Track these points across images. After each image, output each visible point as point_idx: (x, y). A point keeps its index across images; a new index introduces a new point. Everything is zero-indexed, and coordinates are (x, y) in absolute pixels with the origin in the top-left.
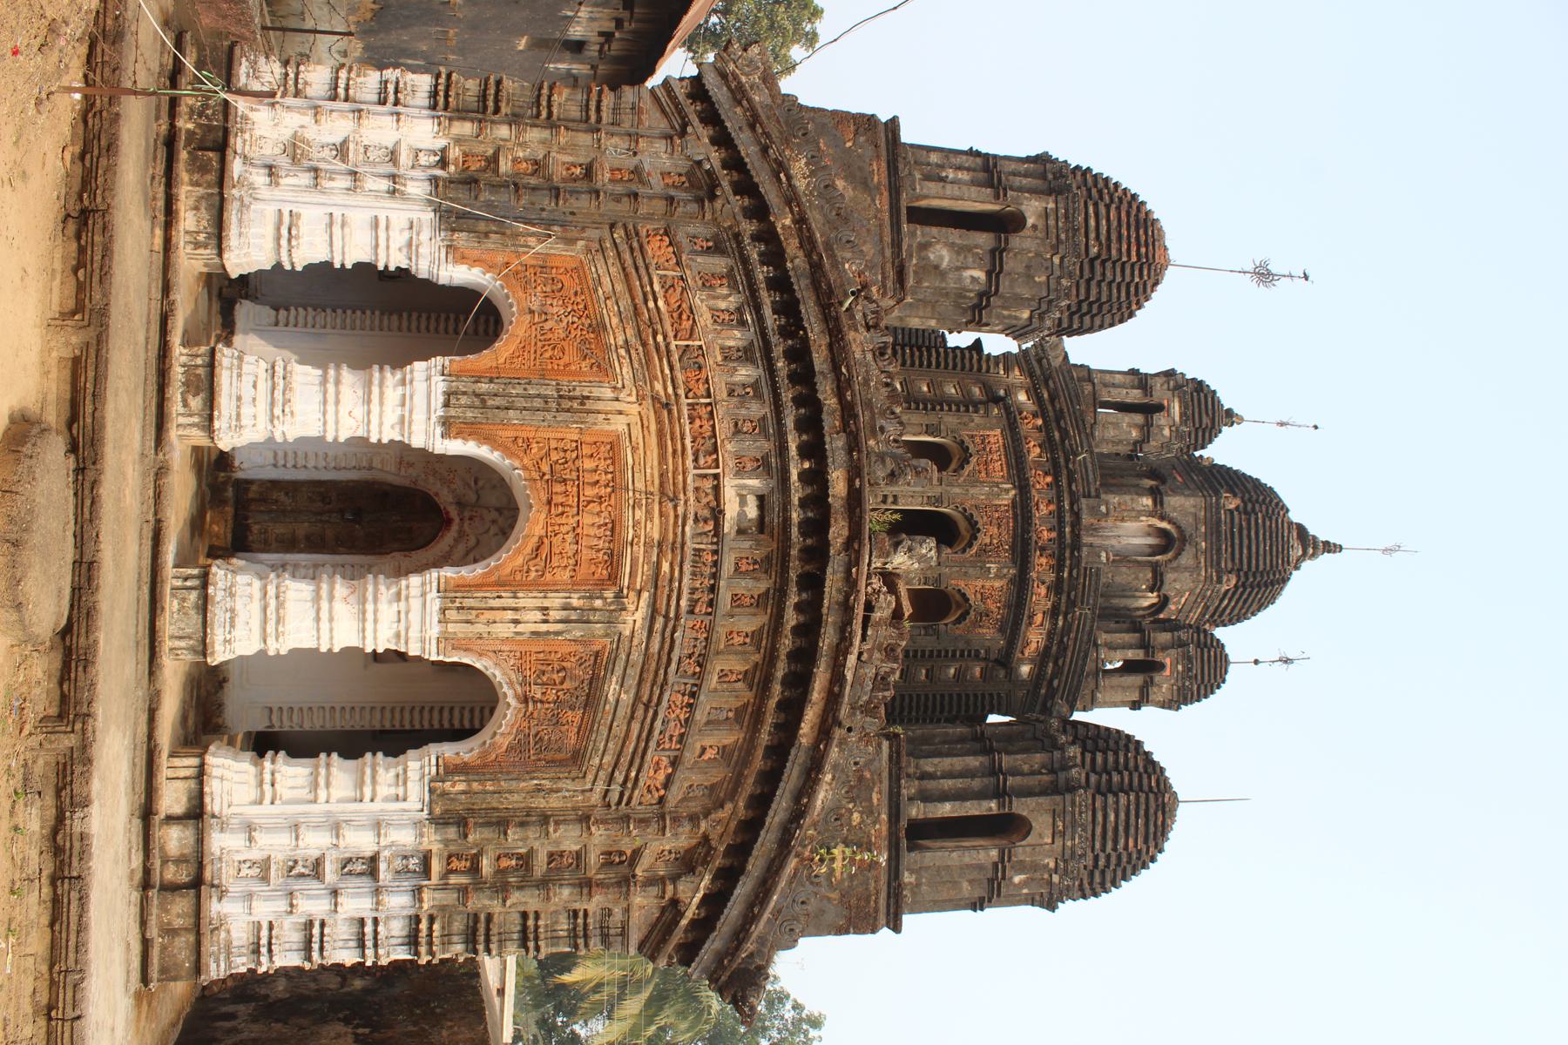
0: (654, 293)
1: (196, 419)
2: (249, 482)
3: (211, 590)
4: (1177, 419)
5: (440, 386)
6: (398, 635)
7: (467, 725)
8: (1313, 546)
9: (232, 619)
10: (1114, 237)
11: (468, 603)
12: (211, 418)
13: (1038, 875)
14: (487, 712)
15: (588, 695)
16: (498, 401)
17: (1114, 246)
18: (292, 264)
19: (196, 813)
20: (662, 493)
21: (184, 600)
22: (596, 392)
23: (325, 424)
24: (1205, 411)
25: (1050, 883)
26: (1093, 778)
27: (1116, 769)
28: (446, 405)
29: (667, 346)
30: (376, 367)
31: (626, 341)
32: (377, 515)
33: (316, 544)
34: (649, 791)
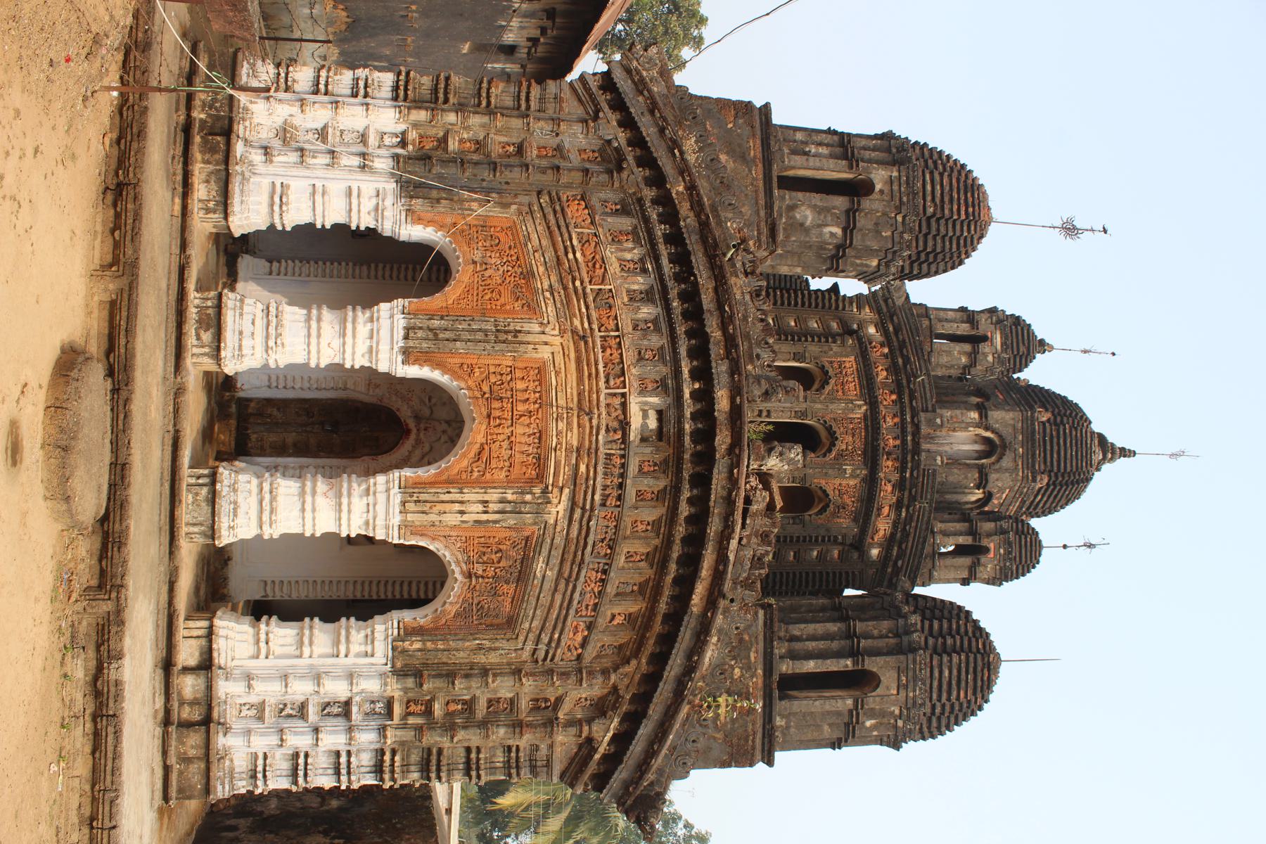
0: (573, 246)
1: (207, 350)
2: (249, 400)
3: (218, 486)
4: (999, 347)
5: (400, 322)
6: (367, 523)
7: (422, 596)
8: (1111, 452)
9: (235, 510)
10: (946, 199)
11: (423, 497)
12: (218, 349)
13: (885, 720)
14: (438, 586)
15: (520, 572)
16: (448, 335)
17: (947, 207)
18: (283, 225)
19: (206, 665)
20: (580, 408)
21: (197, 494)
22: (527, 327)
24: (1022, 341)
25: (896, 727)
26: (931, 641)
27: (950, 634)
28: (406, 337)
29: (584, 289)
30: (350, 307)
31: (551, 286)
32: (350, 426)
33: (301, 450)
34: (569, 650)
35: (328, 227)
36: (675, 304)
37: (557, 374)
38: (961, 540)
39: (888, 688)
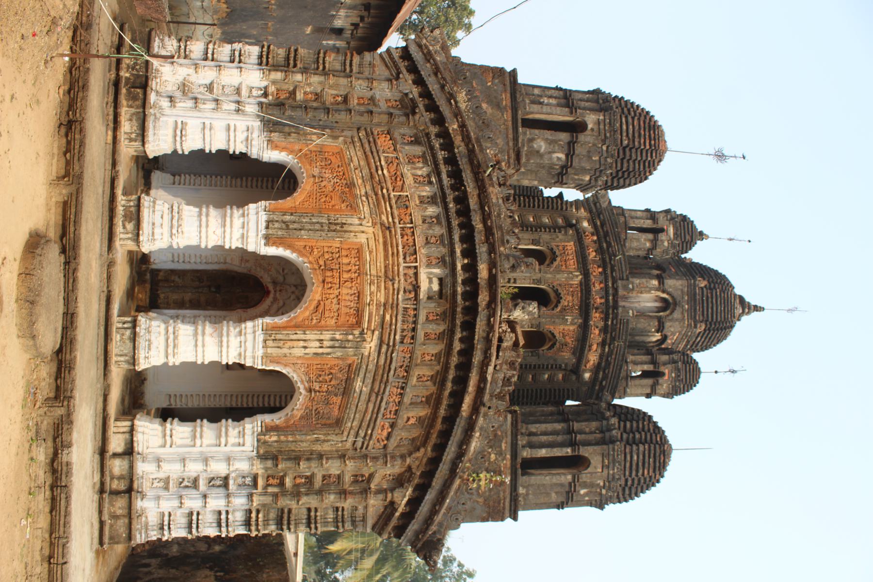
1: (130, 236)
2: (159, 271)
4: (672, 236)
5: (263, 217)
6: (240, 355)
8: (748, 308)
9: (149, 345)
10: (636, 135)
11: (279, 337)
12: (138, 235)
14: (289, 398)
15: (345, 388)
16: (296, 226)
17: (637, 140)
18: (183, 150)
19: (129, 452)
20: (386, 276)
21: (123, 335)
22: (350, 221)
24: (687, 232)
25: (601, 494)
26: (625, 436)
28: (267, 227)
29: (389, 195)
32: (229, 288)
33: (195, 305)
34: (378, 441)
35: (214, 151)
37: (371, 252)
38: (646, 367)
39: (595, 468)
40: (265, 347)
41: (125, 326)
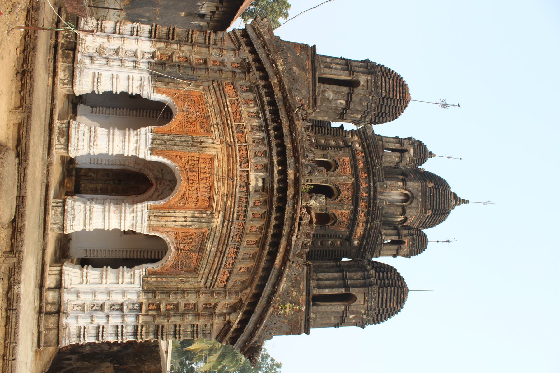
1: (62, 146)
2: (81, 169)
3: (66, 207)
4: (412, 155)
5: (150, 136)
6: (133, 225)
7: (157, 257)
8: (459, 201)
9: (74, 218)
10: (391, 90)
11: (158, 214)
12: (68, 146)
14: (164, 253)
16: (171, 143)
17: (391, 93)
19: (59, 287)
20: (228, 177)
21: (56, 210)
22: (206, 140)
23: (109, 149)
25: (363, 318)
26: (379, 281)
28: (152, 143)
29: (232, 124)
30: (127, 129)
31: (217, 122)
32: (127, 182)
33: (104, 192)
34: (221, 283)
36: (271, 132)
37: (219, 161)
38: (394, 238)
39: (360, 302)
40: (149, 220)
41: (58, 205)
